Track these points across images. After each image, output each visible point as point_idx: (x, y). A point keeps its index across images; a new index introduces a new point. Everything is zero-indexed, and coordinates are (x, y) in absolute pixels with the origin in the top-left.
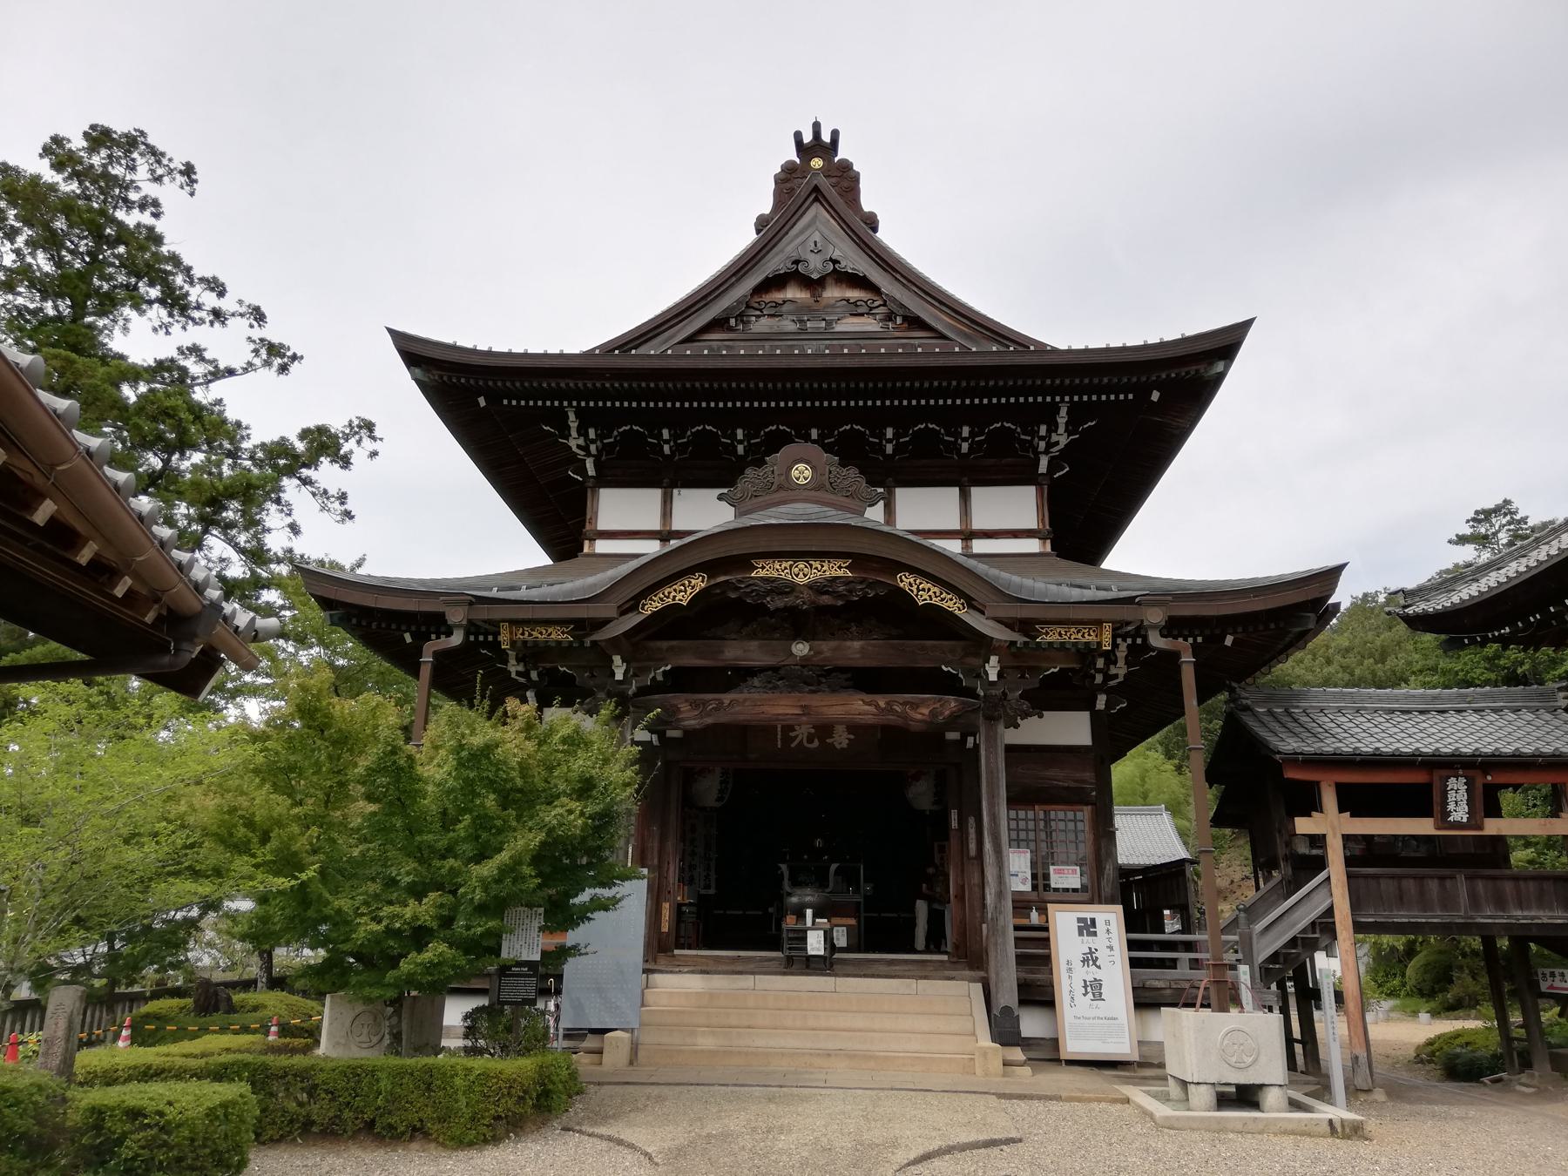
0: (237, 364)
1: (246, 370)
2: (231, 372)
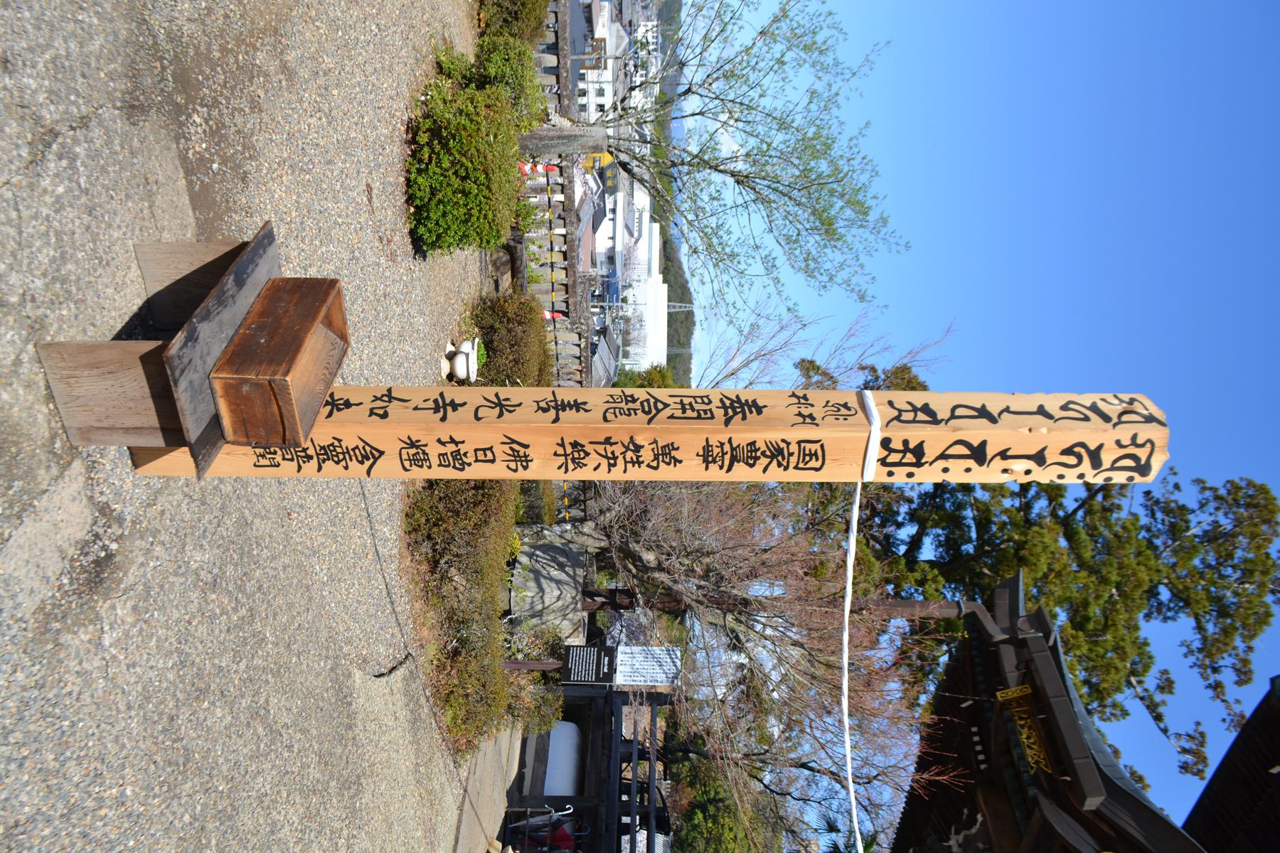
0: (1168, 721)
1: (1165, 731)
2: (1158, 718)
